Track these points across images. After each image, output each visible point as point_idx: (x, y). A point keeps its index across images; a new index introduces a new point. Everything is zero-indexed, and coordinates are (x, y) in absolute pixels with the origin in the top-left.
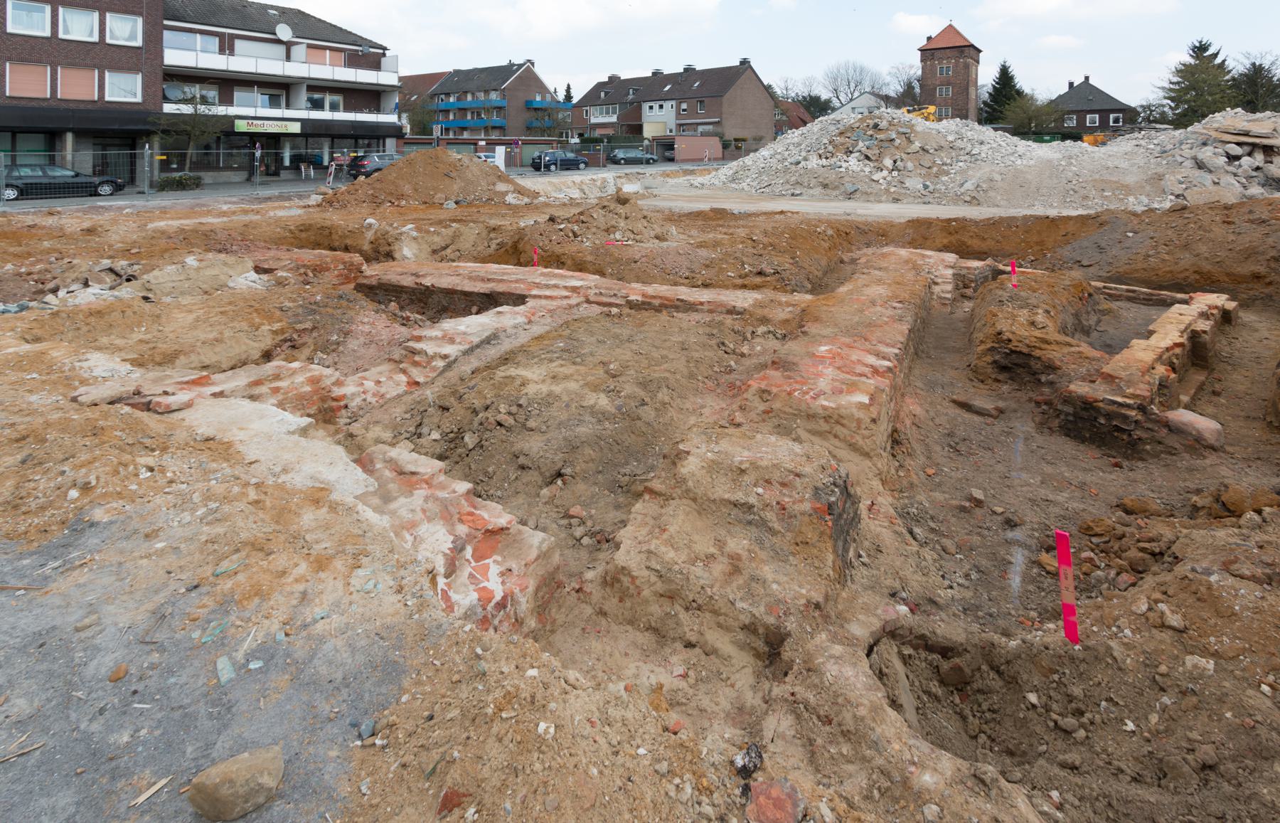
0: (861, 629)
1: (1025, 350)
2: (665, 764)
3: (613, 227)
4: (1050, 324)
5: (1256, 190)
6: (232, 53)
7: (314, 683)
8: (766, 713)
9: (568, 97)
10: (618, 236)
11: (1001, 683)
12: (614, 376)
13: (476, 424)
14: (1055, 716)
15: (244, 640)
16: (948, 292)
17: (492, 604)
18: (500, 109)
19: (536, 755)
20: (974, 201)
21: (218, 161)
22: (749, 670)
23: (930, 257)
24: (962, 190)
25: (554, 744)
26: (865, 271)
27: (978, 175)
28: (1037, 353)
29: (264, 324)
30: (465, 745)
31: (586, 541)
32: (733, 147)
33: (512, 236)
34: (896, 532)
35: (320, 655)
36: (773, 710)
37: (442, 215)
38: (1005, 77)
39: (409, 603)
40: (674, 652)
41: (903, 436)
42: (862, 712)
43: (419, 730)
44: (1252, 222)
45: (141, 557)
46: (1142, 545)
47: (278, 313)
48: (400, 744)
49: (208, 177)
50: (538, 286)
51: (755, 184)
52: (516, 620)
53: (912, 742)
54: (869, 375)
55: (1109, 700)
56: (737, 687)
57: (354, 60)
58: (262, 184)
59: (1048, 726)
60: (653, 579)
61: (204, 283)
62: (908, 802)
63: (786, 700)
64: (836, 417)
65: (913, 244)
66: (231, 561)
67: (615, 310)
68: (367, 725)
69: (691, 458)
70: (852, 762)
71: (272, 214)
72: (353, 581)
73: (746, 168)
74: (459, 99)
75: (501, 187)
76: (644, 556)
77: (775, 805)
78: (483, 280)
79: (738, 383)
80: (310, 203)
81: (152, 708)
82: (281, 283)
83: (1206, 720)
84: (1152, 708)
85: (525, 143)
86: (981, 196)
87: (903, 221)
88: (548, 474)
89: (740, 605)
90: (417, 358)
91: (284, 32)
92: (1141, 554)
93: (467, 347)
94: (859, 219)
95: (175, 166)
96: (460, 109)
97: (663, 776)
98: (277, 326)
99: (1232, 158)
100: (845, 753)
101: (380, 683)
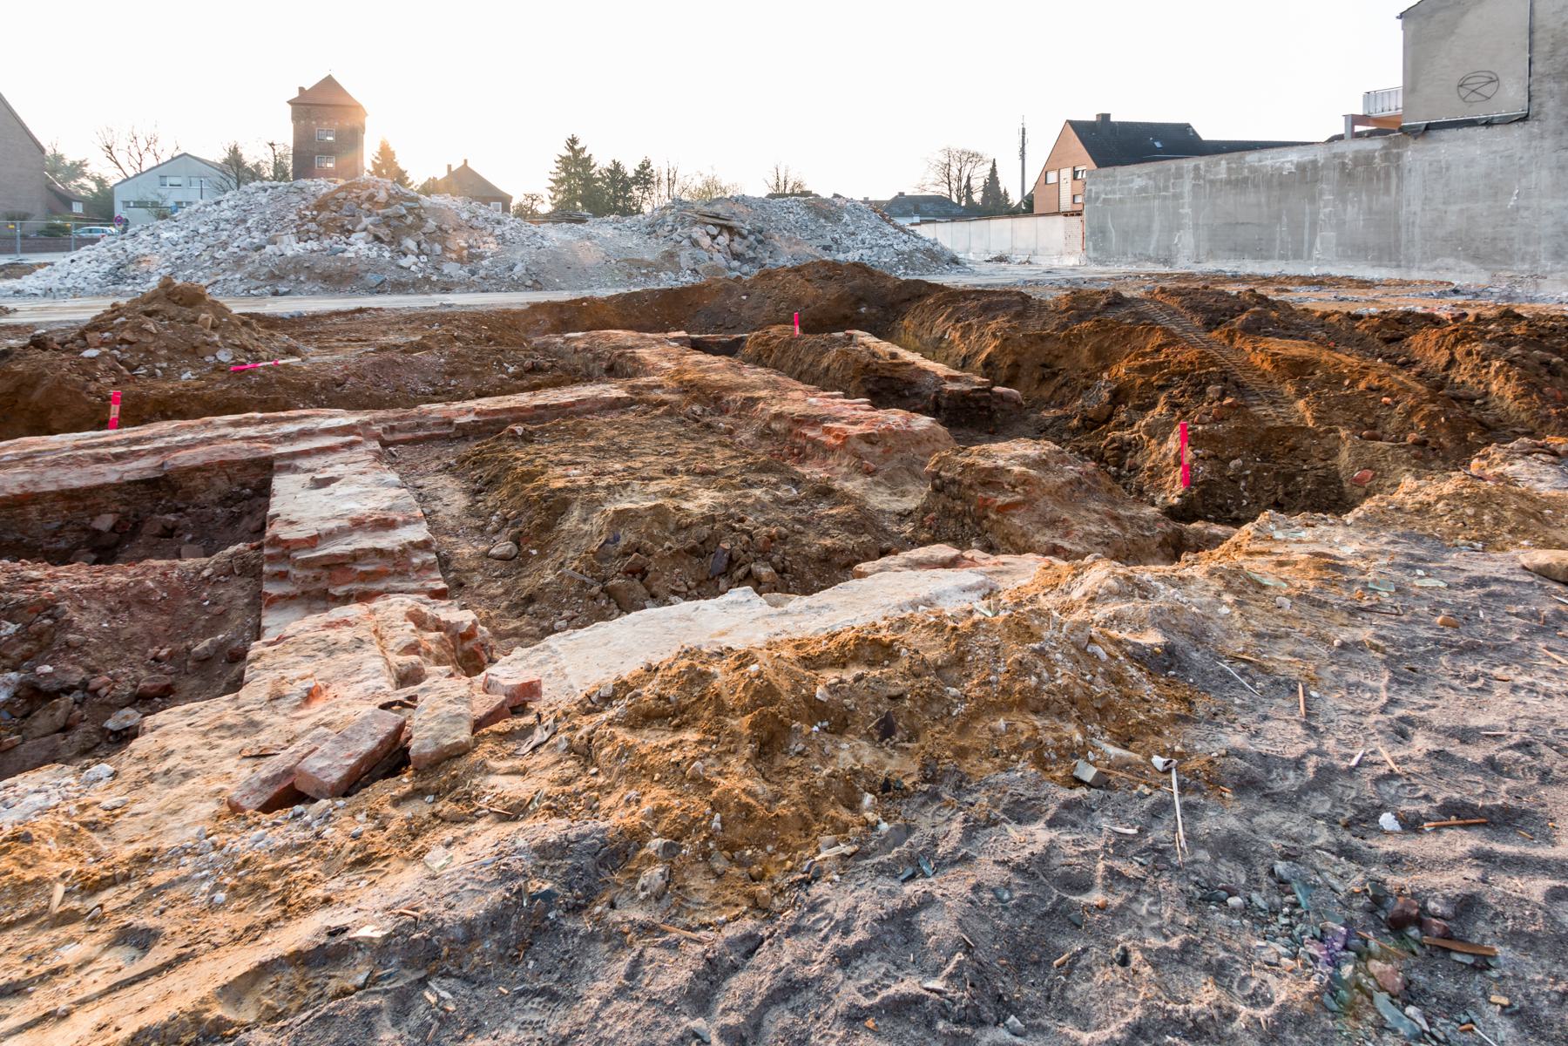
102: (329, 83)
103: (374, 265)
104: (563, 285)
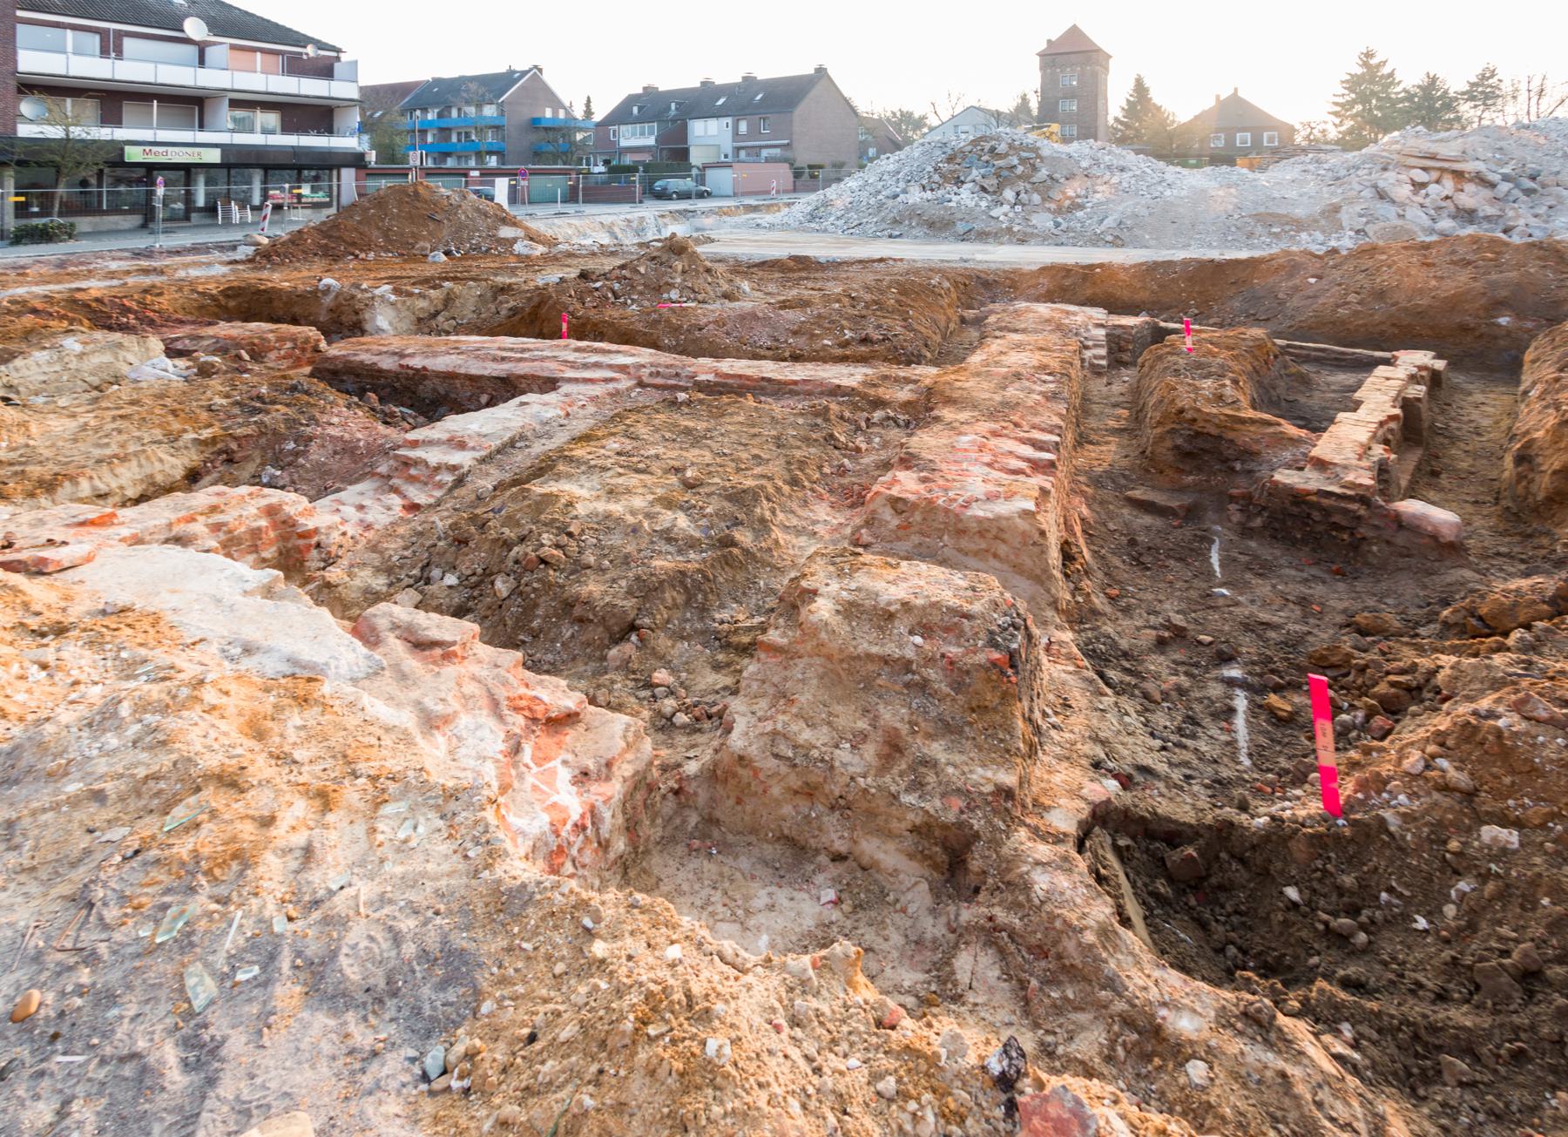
0: (1065, 819)
1: (1214, 431)
2: (891, 1080)
3: (667, 284)
4: (1242, 398)
5: (1446, 224)
6: (119, 54)
7: (344, 995)
8: (956, 946)
9: (588, 113)
10: (674, 294)
11: (1246, 875)
12: (692, 487)
13: (510, 564)
14: (1325, 917)
15: (225, 933)
16: (1102, 358)
17: (569, 826)
18: (497, 128)
19: (710, 1091)
20: (1118, 242)
21: (100, 202)
22: (924, 886)
23: (1074, 314)
24: (1103, 228)
25: (734, 1072)
26: (998, 333)
27: (1120, 208)
28: (1230, 435)
29: (185, 431)
30: (598, 1084)
31: (682, 718)
32: (806, 176)
33: (530, 299)
34: (1086, 679)
35: (345, 950)
36: (966, 943)
37: (429, 271)
38: (1140, 89)
39: (471, 854)
40: (820, 869)
41: (1075, 550)
42: (1090, 937)
43: (519, 1060)
44: (1453, 263)
45: (44, 810)
46: (1392, 678)
47: (204, 415)
48: (492, 1084)
49: (84, 223)
50: (573, 365)
51: (841, 222)
52: (599, 843)
53: (1157, 973)
54: (1028, 471)
55: (1390, 890)
56: (910, 911)
57: (296, 66)
58: (165, 231)
59: (1316, 929)
60: (784, 769)
61: (91, 374)
62: (1164, 1060)
63: (983, 928)
64: (994, 531)
65: (1049, 297)
66: (188, 806)
67: (682, 396)
68: (433, 1057)
69: (820, 601)
70: (1083, 1009)
71: (181, 274)
72: (381, 826)
73: (826, 204)
74: (440, 115)
75: (506, 232)
76: (766, 739)
77: (1055, 1129)
78: (495, 359)
79: (856, 487)
80: (237, 258)
81: (88, 1062)
82: (205, 371)
83: (1518, 910)
84: (1448, 900)
85: (534, 173)
86: (1125, 235)
87: (1034, 268)
88: (616, 629)
89: (908, 799)
90: (413, 471)
91: (194, 28)
92: (1393, 690)
93: (483, 453)
94: (980, 267)
95: (36, 209)
96: (442, 130)
97: (890, 1100)
98: (206, 434)
99: (1418, 186)
100: (1071, 996)
101: (443, 985)
102: (1074, 33)
103: (970, 214)
104: (1152, 243)
